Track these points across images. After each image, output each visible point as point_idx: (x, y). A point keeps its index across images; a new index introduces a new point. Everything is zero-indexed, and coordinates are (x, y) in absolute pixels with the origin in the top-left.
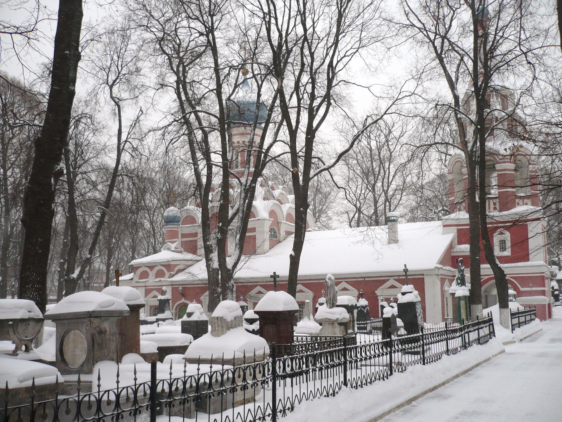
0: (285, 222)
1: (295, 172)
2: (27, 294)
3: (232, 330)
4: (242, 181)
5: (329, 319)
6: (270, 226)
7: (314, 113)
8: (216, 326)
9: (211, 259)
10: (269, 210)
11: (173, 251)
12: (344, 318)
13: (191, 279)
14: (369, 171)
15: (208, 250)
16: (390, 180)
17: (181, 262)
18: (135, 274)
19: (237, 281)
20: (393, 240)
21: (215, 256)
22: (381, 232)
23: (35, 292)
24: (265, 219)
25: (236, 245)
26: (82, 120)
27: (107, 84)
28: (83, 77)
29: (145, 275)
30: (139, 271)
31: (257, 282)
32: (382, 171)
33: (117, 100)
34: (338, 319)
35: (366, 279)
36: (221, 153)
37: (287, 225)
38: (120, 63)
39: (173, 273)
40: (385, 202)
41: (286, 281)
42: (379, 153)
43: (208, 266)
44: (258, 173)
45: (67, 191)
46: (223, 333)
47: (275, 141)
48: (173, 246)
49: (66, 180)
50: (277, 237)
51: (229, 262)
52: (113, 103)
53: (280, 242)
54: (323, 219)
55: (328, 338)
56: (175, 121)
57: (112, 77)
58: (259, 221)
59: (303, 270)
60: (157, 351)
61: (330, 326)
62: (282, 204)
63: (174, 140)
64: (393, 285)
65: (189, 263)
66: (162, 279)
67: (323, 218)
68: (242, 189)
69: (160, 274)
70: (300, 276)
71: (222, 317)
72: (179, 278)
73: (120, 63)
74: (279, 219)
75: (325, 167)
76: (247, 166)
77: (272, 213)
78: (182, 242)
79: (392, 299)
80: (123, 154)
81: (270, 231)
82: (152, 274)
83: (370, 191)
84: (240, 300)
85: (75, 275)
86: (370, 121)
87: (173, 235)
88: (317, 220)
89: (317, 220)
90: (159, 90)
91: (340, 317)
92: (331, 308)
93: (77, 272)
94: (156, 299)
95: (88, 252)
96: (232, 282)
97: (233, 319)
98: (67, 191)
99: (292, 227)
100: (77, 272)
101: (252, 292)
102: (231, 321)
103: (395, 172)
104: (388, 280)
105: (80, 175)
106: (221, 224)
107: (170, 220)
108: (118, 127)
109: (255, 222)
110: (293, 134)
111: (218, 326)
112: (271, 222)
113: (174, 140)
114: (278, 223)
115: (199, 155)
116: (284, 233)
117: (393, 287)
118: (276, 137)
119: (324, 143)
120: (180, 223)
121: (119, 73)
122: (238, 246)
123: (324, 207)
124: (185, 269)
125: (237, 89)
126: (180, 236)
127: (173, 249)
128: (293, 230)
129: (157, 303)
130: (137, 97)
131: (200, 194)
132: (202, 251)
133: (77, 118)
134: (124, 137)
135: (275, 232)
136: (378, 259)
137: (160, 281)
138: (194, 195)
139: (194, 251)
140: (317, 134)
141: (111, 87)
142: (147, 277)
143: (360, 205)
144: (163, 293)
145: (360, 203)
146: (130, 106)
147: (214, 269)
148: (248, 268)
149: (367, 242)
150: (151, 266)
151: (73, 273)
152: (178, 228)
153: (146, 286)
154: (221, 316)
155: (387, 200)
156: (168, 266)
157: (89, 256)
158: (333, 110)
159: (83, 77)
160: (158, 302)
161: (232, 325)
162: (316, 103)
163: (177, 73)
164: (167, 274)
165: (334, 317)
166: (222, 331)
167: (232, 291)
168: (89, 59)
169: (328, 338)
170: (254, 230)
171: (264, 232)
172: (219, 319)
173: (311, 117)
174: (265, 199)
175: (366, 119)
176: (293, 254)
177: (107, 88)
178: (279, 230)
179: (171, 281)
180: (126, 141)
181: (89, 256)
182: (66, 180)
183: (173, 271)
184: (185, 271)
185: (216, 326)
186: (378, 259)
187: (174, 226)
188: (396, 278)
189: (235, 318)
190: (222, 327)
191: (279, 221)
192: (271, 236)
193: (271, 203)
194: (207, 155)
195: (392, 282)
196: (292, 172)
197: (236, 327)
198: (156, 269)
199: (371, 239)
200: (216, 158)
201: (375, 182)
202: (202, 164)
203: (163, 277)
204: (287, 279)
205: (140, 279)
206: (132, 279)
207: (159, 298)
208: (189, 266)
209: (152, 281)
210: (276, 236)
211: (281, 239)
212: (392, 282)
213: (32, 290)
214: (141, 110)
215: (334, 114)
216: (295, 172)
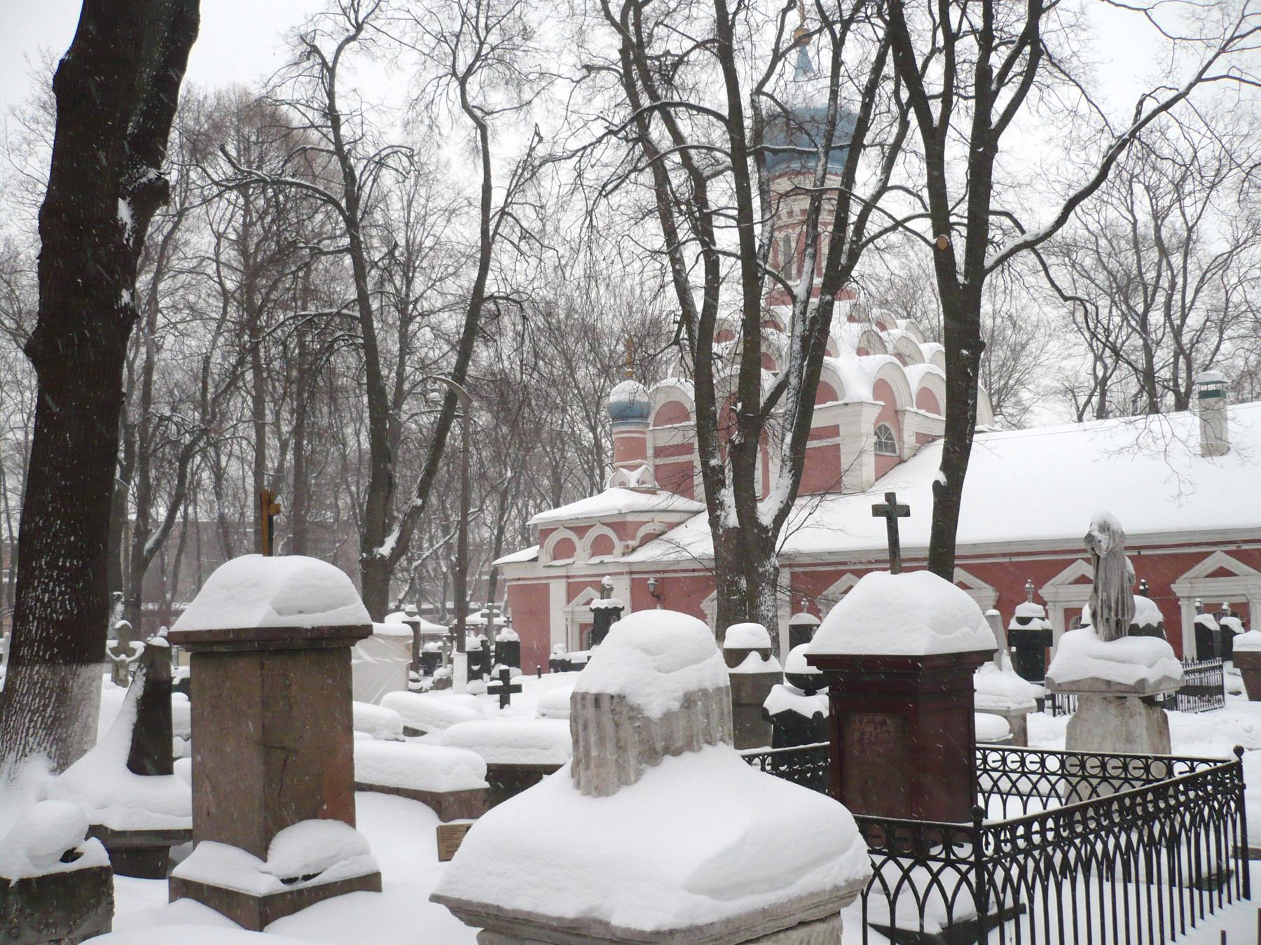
0: (915, 409)
1: (943, 246)
2: (35, 590)
3: (669, 761)
4: (795, 291)
5: (1108, 682)
6: (877, 421)
7: (994, 87)
8: (593, 739)
9: (721, 503)
10: (873, 380)
11: (633, 490)
12: (1166, 678)
13: (673, 556)
14: (1130, 281)
15: (713, 482)
16: (1188, 300)
17: (652, 515)
18: (542, 547)
19: (790, 561)
20: (1214, 446)
21: (727, 495)
22: (1188, 424)
23: (58, 582)
24: (861, 403)
25: (783, 461)
26: (390, 162)
27: (454, 74)
28: (389, 56)
29: (564, 549)
30: (554, 539)
31: (845, 563)
32: (1166, 274)
33: (479, 113)
34: (1142, 682)
35: (1144, 552)
36: (735, 213)
37: (918, 419)
38: (482, 21)
39: (632, 543)
40: (1176, 357)
41: (924, 559)
42: (1158, 229)
43: (714, 522)
44: (836, 279)
45: (361, 341)
46: (624, 778)
47: (883, 188)
48: (633, 477)
49: (358, 314)
50: (894, 451)
51: (766, 512)
52: (470, 122)
53: (902, 461)
54: (1010, 410)
55: (1112, 763)
56: (611, 132)
57: (465, 58)
58: (848, 409)
59: (969, 531)
60: (487, 785)
61: (1112, 709)
62: (905, 364)
63: (610, 187)
64: (1221, 568)
65: (674, 518)
66: (607, 559)
67: (1008, 408)
68: (797, 312)
69: (603, 545)
70: (962, 546)
71: (622, 698)
72: (649, 554)
73: (482, 21)
74: (898, 402)
75: (1028, 237)
76: (810, 250)
77: (881, 388)
78: (657, 467)
79: (1225, 607)
80: (495, 247)
81: (876, 434)
82: (582, 545)
83: (1134, 329)
84: (801, 611)
85: (385, 550)
86: (1150, 106)
87: (632, 450)
88: (996, 409)
89: (996, 409)
90: (583, 85)
91: (1152, 675)
92: (1110, 638)
93: (391, 542)
94: (587, 608)
95: (415, 493)
96: (774, 561)
97: (675, 706)
98: (361, 341)
99: (937, 422)
100: (391, 542)
101: (831, 589)
102: (668, 716)
103: (1202, 278)
104: (1208, 554)
105: (418, 319)
106: (740, 405)
107: (625, 413)
108: (481, 181)
109: (838, 411)
110: (935, 138)
111: (601, 742)
112: (878, 411)
113: (610, 187)
114: (896, 414)
115: (684, 230)
116: (914, 439)
117: (1222, 573)
118: (887, 178)
119: (1020, 185)
120: (651, 420)
121: (482, 43)
122: (789, 464)
123: (1011, 382)
124: (664, 533)
125: (780, 65)
126: (650, 452)
127: (633, 484)
128: (940, 429)
129: (590, 619)
130: (530, 102)
131: (691, 338)
132: (700, 490)
133: (377, 159)
134: (498, 200)
135: (890, 437)
136: (1180, 495)
137: (602, 562)
138: (677, 342)
139: (688, 492)
140: (1003, 142)
141: (463, 83)
142: (570, 555)
143: (1105, 373)
144: (606, 592)
145: (1106, 367)
146: (512, 130)
147: (728, 531)
148: (819, 525)
149: (1145, 451)
150: (580, 529)
151: (382, 544)
152: (643, 433)
153: (568, 577)
154: (612, 690)
155: (1179, 350)
156: (621, 526)
157: (419, 502)
158: (1041, 98)
159: (389, 56)
160: (592, 615)
161: (668, 738)
162: (996, 61)
163: (621, 28)
164: (619, 546)
165: (1127, 675)
166: (621, 767)
167: (774, 584)
168: (408, 16)
169: (1112, 763)
170: (834, 431)
171: (860, 435)
172: (606, 705)
173: (985, 98)
174: (861, 352)
175: (1141, 103)
176: (942, 478)
177: (455, 84)
178: (900, 431)
179: (630, 564)
180: (503, 212)
181: (419, 502)
182: (358, 314)
183: (633, 538)
184: (662, 537)
185: (593, 739)
186: (1180, 495)
187: (633, 428)
188: (1233, 547)
189: (689, 701)
190: (620, 747)
191: (899, 407)
192: (879, 445)
193: (876, 361)
194: (704, 232)
195: (1219, 559)
196: (935, 247)
197: (690, 745)
198: (591, 535)
199: (1161, 442)
200: (727, 237)
201: (1147, 308)
202: (691, 252)
203: (610, 552)
204: (926, 554)
205: (555, 559)
206: (535, 559)
207: (594, 605)
208: (672, 526)
209: (582, 562)
210: (893, 446)
211: (906, 453)
212: (1219, 559)
213: (51, 578)
214: (537, 134)
215: (1043, 108)
216: (943, 246)
